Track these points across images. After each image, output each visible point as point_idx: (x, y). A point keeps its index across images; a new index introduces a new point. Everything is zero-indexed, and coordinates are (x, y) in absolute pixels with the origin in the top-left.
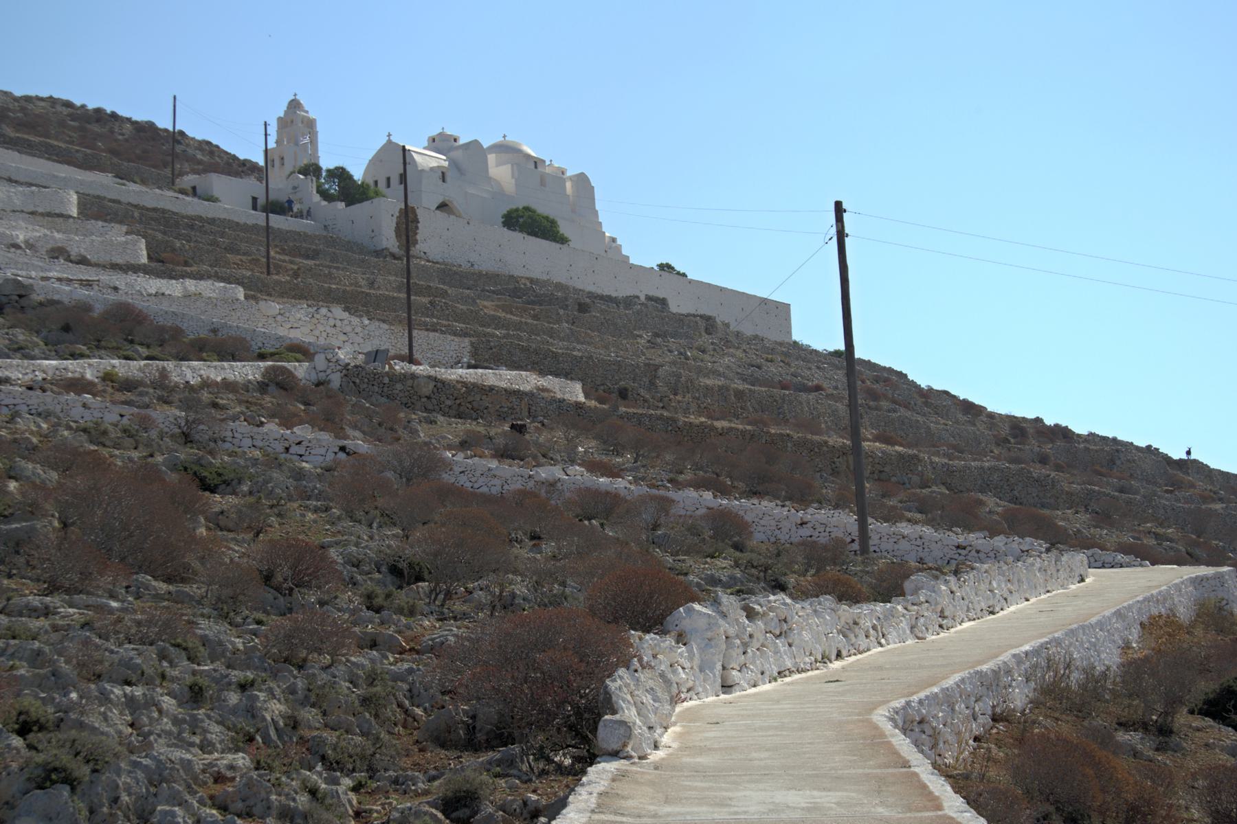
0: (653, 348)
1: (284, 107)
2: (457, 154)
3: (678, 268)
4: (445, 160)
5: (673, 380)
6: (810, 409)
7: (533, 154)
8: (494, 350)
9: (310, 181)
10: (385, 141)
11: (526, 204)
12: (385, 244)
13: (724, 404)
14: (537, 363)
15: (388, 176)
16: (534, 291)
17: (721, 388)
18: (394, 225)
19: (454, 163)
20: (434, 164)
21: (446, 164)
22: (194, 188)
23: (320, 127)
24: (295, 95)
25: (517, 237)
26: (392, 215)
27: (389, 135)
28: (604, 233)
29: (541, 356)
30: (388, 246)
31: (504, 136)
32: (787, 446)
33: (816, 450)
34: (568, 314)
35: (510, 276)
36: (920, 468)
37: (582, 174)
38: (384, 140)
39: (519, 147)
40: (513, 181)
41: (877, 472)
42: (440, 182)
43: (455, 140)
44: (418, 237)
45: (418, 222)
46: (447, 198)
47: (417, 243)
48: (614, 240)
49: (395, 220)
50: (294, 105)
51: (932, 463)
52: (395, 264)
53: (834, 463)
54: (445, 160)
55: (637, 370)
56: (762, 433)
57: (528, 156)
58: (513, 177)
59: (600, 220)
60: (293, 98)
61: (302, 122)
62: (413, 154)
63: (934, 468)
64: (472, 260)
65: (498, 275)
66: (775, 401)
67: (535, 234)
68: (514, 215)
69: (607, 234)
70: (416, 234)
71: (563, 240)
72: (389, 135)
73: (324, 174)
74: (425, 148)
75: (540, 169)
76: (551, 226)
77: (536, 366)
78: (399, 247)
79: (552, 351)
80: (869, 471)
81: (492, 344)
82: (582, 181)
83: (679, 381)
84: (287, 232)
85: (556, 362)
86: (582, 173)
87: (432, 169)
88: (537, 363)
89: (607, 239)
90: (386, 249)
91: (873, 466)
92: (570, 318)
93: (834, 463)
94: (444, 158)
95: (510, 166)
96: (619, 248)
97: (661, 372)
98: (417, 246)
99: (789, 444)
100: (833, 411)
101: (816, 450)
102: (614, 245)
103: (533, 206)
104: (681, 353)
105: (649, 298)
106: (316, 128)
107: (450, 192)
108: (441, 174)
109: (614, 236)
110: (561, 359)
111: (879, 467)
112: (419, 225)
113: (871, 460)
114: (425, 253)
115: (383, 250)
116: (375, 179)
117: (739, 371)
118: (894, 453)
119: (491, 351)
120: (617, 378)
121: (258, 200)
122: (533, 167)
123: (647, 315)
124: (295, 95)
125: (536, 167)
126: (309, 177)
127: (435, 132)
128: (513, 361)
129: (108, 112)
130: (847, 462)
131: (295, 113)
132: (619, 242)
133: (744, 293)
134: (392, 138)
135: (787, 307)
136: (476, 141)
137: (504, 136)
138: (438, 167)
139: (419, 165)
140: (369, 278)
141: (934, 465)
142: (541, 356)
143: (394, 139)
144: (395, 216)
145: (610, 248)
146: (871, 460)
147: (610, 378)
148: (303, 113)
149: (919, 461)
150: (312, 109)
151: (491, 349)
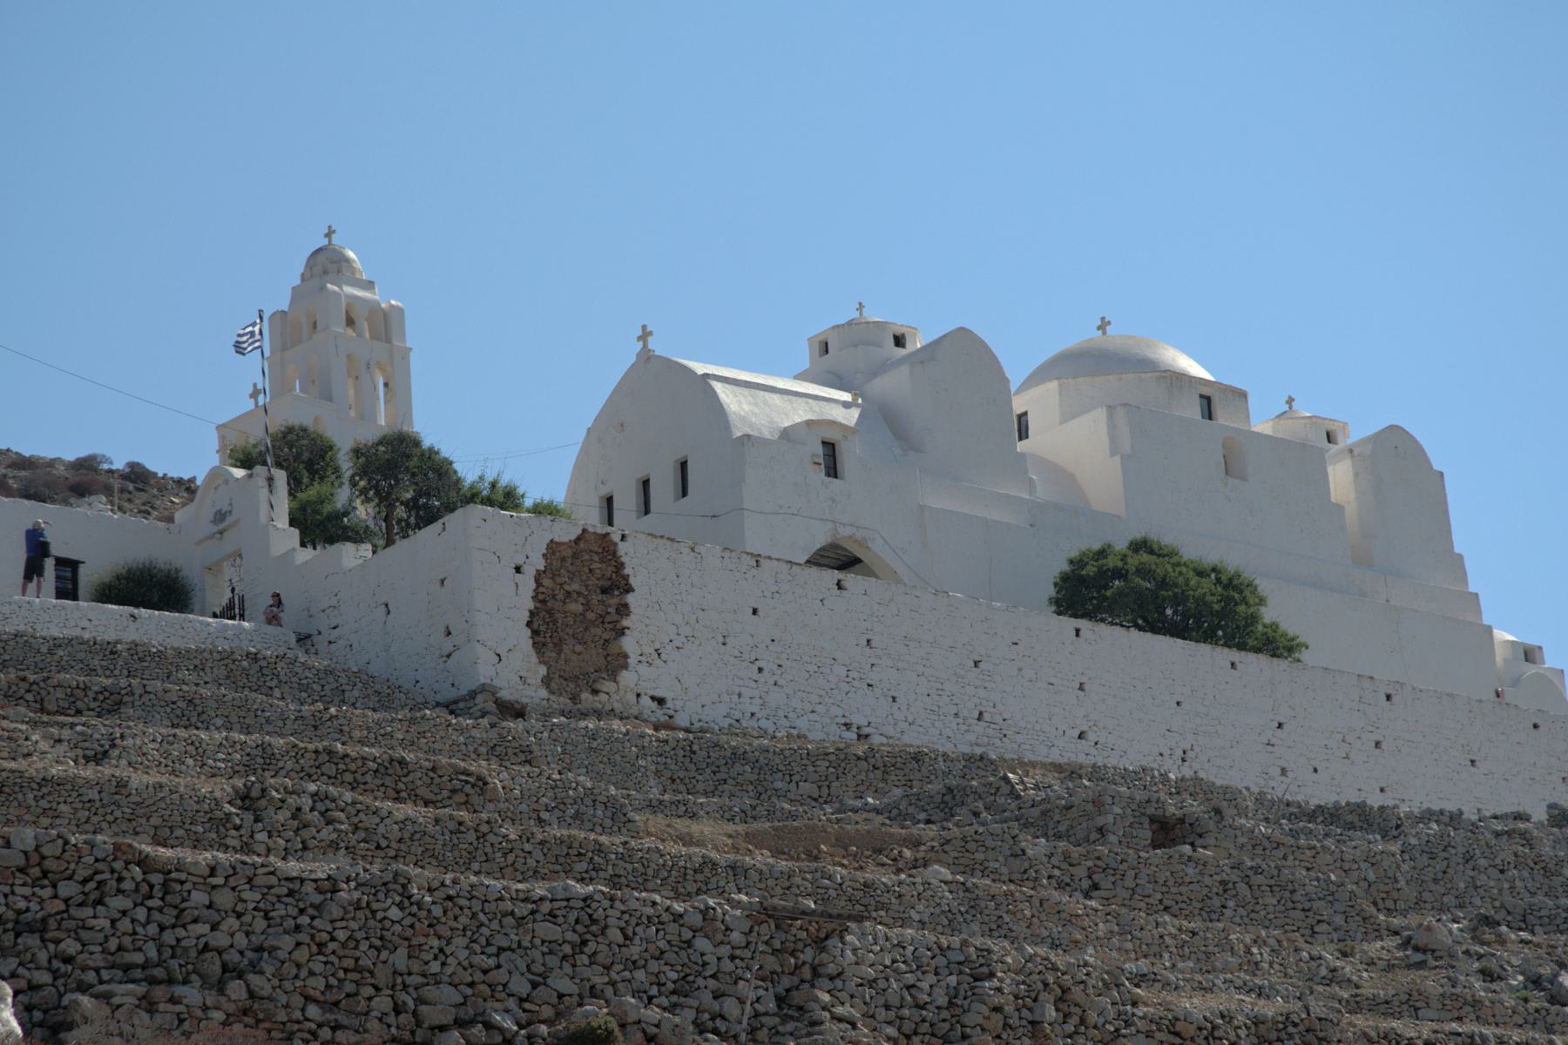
0: (1421, 965)
2: (894, 385)
4: (846, 405)
10: (631, 359)
11: (1138, 535)
12: (485, 672)
15: (642, 475)
20: (799, 414)
21: (851, 417)
23: (415, 336)
26: (518, 569)
27: (645, 335)
28: (1488, 630)
29: (67, 889)
31: (1103, 325)
34: (1066, 856)
35: (969, 759)
43: (899, 341)
45: (629, 589)
46: (844, 531)
47: (625, 667)
48: (1530, 654)
49: (527, 583)
52: (461, 730)
55: (701, 943)
57: (1180, 380)
59: (1472, 588)
60: (325, 242)
61: (350, 322)
62: (718, 387)
64: (857, 719)
65: (917, 757)
67: (1178, 631)
69: (1502, 635)
70: (621, 632)
71: (1277, 646)
72: (645, 335)
73: (346, 465)
74: (801, 377)
75: (1223, 418)
76: (1228, 600)
77: (32, 941)
78: (546, 682)
79: (143, 862)
84: (57, 644)
86: (1394, 429)
88: (39, 928)
89: (1500, 655)
90: (483, 688)
92: (1081, 872)
94: (846, 396)
95: (1100, 414)
98: (626, 678)
102: (1531, 670)
103: (1166, 537)
104: (1536, 982)
106: (403, 337)
108: (820, 449)
109: (1532, 641)
110: (199, 897)
114: (660, 701)
115: (473, 694)
116: (604, 491)
120: (566, 985)
121: (82, 570)
124: (329, 234)
126: (259, 469)
129: (119, 464)
131: (323, 288)
132: (1551, 660)
134: (652, 343)
135: (809, 339)
142: (67, 889)
143: (657, 346)
145: (1516, 682)
147: (521, 986)
148: (348, 290)
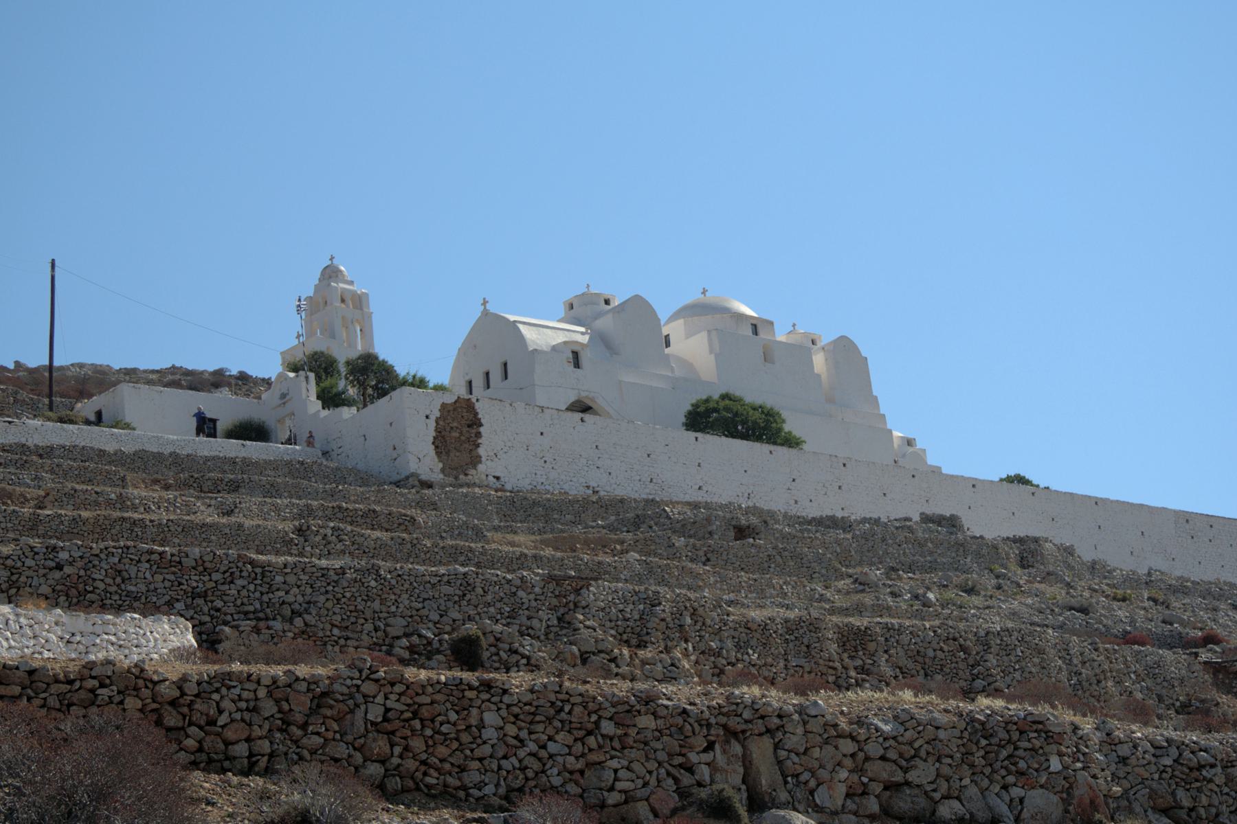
0: (863, 591)
1: (315, 279)
2: (604, 323)
3: (1035, 482)
4: (583, 333)
5: (633, 612)
6: (1070, 663)
7: (749, 312)
8: (68, 570)
9: (303, 379)
12: (413, 467)
13: (802, 662)
14: (204, 595)
16: (668, 517)
17: (791, 627)
18: (432, 433)
19: (602, 340)
20: (560, 338)
21: (585, 339)
22: (99, 414)
24: (332, 258)
25: (716, 446)
26: (427, 417)
27: (485, 302)
28: (890, 432)
30: (419, 472)
31: (704, 292)
32: (481, 726)
33: (608, 727)
34: (694, 546)
35: (647, 501)
36: (1055, 764)
37: (843, 338)
38: (477, 312)
39: (728, 305)
40: (713, 356)
41: (877, 788)
42: (571, 368)
43: (607, 302)
44: (481, 451)
45: (481, 425)
46: (583, 394)
47: (480, 462)
48: (910, 442)
49: (432, 424)
50: (331, 273)
51: (1110, 742)
52: (402, 495)
53: (690, 770)
54: (583, 333)
55: (521, 593)
56: (368, 687)
57: (741, 317)
58: (711, 352)
59: (882, 412)
60: (330, 262)
62: (521, 327)
63: (1123, 760)
64: (593, 484)
65: (622, 501)
66: (963, 648)
68: (702, 409)
70: (478, 446)
71: (791, 442)
72: (485, 302)
73: (343, 370)
74: (561, 321)
75: (763, 334)
76: (767, 421)
77: (200, 601)
78: (443, 471)
80: (842, 789)
81: (63, 556)
82: (845, 351)
83: (653, 614)
85: (265, 589)
87: (554, 348)
88: (204, 595)
89: (896, 443)
90: (413, 475)
91: (858, 770)
92: (701, 553)
93: (690, 770)
94: (582, 329)
95: (704, 334)
96: (920, 456)
97: (596, 593)
98: (481, 467)
99: (490, 718)
100: (1148, 668)
101: (608, 727)
102: (911, 449)
104: (916, 597)
105: (926, 519)
106: (368, 307)
107: (588, 384)
108: (571, 355)
109: (911, 436)
111: (886, 772)
112: (482, 429)
113: (848, 747)
114: (498, 478)
115: (407, 478)
116: (467, 378)
117: (1036, 619)
118: (943, 719)
119: (57, 575)
120: (456, 615)
121: (218, 424)
122: (749, 332)
123: (884, 540)
125: (756, 332)
126: (301, 373)
127: (570, 294)
128: (129, 594)
129: (234, 372)
130: (746, 761)
131: (329, 285)
132: (920, 445)
133: (1142, 505)
134: (488, 306)
136: (637, 296)
137: (704, 292)
138: (565, 343)
139: (528, 342)
140: (222, 504)
141: (1124, 750)
142: (216, 576)
144: (433, 418)
145: (904, 456)
146: (848, 747)
147: (436, 617)
148: (341, 285)
149: (1051, 737)
150: (356, 276)
151: (59, 567)
